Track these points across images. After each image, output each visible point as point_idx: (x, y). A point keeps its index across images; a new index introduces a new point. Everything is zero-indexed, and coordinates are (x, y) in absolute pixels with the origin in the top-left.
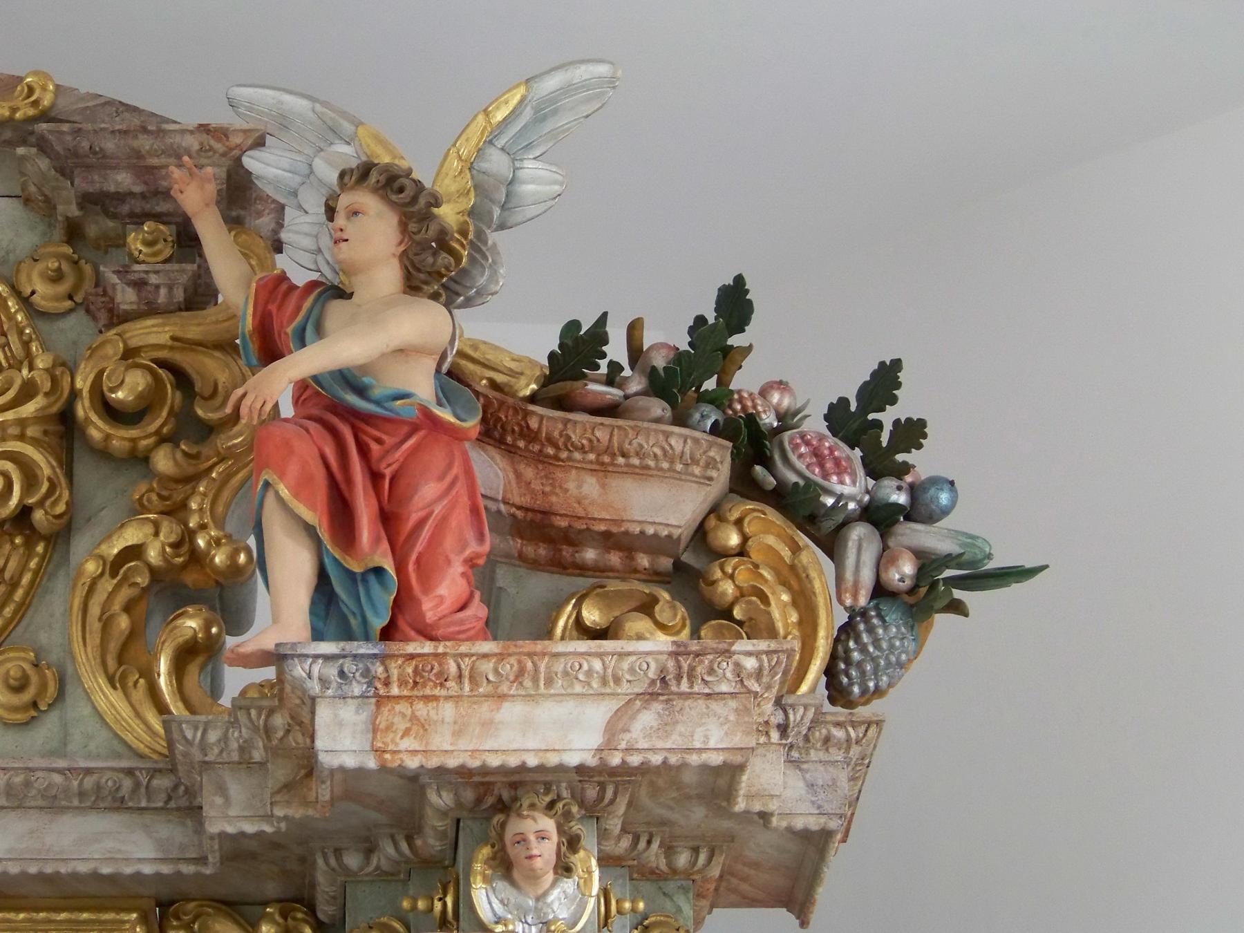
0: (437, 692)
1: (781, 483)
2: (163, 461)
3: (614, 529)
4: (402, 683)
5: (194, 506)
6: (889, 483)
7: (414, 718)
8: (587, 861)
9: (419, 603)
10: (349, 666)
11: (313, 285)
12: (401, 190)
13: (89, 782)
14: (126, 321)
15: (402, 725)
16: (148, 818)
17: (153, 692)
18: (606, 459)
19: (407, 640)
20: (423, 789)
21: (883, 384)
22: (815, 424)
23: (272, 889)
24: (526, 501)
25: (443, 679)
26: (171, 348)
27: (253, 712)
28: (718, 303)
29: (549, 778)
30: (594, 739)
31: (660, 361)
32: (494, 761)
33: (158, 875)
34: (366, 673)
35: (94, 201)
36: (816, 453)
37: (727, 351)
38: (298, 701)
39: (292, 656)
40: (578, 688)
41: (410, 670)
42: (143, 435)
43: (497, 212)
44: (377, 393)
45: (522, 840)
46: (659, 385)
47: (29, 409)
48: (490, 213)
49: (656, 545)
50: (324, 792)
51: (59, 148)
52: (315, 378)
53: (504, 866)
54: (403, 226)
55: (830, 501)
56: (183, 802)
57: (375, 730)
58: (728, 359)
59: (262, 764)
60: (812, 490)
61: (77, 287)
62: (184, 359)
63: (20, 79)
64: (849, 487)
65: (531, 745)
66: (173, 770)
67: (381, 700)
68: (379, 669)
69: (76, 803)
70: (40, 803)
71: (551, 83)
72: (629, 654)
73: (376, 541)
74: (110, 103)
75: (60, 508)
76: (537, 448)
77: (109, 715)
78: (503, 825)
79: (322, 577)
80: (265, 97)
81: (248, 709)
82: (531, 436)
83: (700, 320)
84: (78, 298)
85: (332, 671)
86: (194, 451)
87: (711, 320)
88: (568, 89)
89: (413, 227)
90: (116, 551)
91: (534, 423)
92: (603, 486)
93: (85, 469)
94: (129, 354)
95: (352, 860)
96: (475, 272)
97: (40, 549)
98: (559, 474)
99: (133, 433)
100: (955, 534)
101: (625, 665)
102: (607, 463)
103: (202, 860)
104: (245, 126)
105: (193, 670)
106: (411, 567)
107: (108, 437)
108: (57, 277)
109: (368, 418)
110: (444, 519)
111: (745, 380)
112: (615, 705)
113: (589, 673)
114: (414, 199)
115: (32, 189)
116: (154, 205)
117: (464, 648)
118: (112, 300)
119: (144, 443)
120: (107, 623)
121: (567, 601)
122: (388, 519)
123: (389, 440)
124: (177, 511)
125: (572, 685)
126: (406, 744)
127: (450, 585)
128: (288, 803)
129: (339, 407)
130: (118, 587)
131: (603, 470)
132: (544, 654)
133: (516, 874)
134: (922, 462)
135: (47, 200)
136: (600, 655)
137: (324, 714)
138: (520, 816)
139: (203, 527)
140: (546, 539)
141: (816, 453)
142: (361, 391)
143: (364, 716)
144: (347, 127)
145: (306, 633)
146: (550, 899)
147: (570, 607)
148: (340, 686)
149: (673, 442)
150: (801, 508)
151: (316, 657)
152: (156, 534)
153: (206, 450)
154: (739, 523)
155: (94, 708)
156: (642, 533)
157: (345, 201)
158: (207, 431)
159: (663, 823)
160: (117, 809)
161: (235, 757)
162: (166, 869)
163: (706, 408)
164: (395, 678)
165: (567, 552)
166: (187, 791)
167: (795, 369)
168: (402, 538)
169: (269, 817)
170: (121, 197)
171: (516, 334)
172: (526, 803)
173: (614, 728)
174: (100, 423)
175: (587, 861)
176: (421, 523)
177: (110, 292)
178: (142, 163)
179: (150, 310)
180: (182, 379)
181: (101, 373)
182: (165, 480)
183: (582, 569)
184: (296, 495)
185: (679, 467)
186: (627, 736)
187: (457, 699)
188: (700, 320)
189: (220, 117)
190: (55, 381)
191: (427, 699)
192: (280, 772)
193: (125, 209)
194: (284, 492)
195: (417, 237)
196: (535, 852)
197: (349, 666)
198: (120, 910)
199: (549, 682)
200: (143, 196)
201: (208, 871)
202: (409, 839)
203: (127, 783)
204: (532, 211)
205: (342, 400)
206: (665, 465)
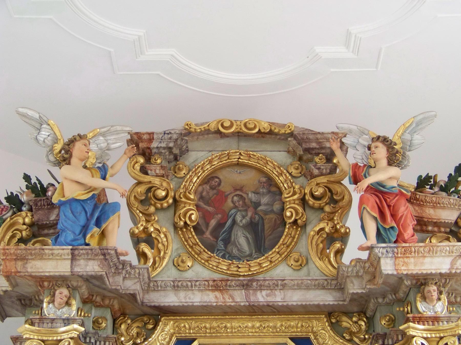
0: (409, 255)
2: (327, 209)
3: (438, 221)
4: (401, 254)
5: (335, 218)
7: (404, 262)
8: (444, 297)
9: (404, 234)
10: (389, 250)
12: (387, 141)
13: (317, 282)
14: (315, 177)
15: (401, 264)
16: (331, 291)
17: (330, 261)
18: (435, 205)
19: (400, 243)
20: (403, 280)
23: (355, 309)
25: (411, 252)
26: (327, 183)
27: (361, 263)
28: (455, 170)
29: (433, 277)
30: (448, 266)
32: (425, 272)
33: (333, 304)
34: (393, 251)
35: (307, 150)
37: (458, 181)
38: (374, 259)
39: (375, 247)
40: (443, 254)
41: (403, 250)
42: (321, 203)
43: (408, 147)
45: (429, 292)
47: (296, 197)
48: (406, 148)
49: (445, 225)
50: (381, 281)
51: (299, 138)
52: (371, 184)
53: (424, 298)
54: (388, 150)
56: (339, 287)
57: (395, 265)
59: (361, 276)
60: (171, 334)
62: (331, 186)
65: (433, 268)
66: (337, 279)
67: (396, 258)
68: (396, 250)
69: (313, 287)
70: (305, 288)
72: (455, 246)
73: (391, 221)
74: (307, 129)
75: (304, 220)
76: (419, 202)
77: (319, 267)
78: (424, 288)
79: (378, 230)
81: (360, 262)
82: (417, 200)
83: (450, 175)
84: (302, 173)
85: (384, 251)
86: (334, 206)
87: (453, 175)
89: (390, 150)
90: (318, 229)
91: (418, 197)
92: (435, 211)
93: (307, 209)
95: (380, 300)
96: (404, 161)
97: (299, 229)
98: (424, 209)
99: (320, 202)
101: (455, 248)
102: (435, 206)
103: (344, 301)
104: (342, 132)
105: (338, 256)
106: (400, 226)
107: (314, 203)
108: (297, 169)
109: (386, 193)
110: (406, 216)
112: (452, 258)
113: (446, 251)
115: (291, 149)
117: (416, 245)
118: (312, 173)
119: (322, 205)
120: (317, 245)
121: (427, 238)
122: (393, 216)
123: (391, 198)
124: (332, 220)
125: (441, 254)
126: (403, 268)
127: (410, 231)
128: (370, 285)
129: (377, 190)
130: (319, 237)
131: (434, 207)
132: (435, 246)
133: (427, 300)
135: (294, 151)
136: (449, 246)
137: (382, 261)
138: (428, 286)
139: (338, 223)
140: (422, 225)
142: (384, 187)
143: (392, 261)
144: (366, 132)
145: (376, 243)
146: (436, 306)
147: (428, 240)
148: (386, 254)
149: (451, 200)
151: (381, 247)
152: (328, 225)
153: (337, 206)
155: (316, 265)
156: (445, 222)
157: (373, 145)
158: (336, 202)
159: (456, 290)
160: (323, 289)
161: (355, 274)
162: (336, 303)
164: (399, 252)
165: (424, 228)
166: (340, 284)
168: (397, 220)
169: (364, 289)
170: (313, 149)
172: (430, 283)
173: (453, 263)
174: (312, 200)
175: (444, 297)
176: (402, 216)
177: (311, 171)
178: (318, 141)
179: (322, 174)
180: (330, 191)
181: (312, 189)
182: (329, 213)
183: (428, 232)
184: (371, 210)
185: (452, 206)
186: (456, 266)
187: (414, 257)
188: (450, 175)
189: (336, 130)
190: (301, 191)
191: (407, 257)
192: (367, 278)
193: (314, 152)
195: (391, 153)
196: (433, 294)
197: (389, 250)
198: (320, 315)
199: (436, 253)
200: (318, 149)
201: (345, 303)
202: (395, 294)
203: (326, 283)
205: (378, 188)
206: (449, 206)
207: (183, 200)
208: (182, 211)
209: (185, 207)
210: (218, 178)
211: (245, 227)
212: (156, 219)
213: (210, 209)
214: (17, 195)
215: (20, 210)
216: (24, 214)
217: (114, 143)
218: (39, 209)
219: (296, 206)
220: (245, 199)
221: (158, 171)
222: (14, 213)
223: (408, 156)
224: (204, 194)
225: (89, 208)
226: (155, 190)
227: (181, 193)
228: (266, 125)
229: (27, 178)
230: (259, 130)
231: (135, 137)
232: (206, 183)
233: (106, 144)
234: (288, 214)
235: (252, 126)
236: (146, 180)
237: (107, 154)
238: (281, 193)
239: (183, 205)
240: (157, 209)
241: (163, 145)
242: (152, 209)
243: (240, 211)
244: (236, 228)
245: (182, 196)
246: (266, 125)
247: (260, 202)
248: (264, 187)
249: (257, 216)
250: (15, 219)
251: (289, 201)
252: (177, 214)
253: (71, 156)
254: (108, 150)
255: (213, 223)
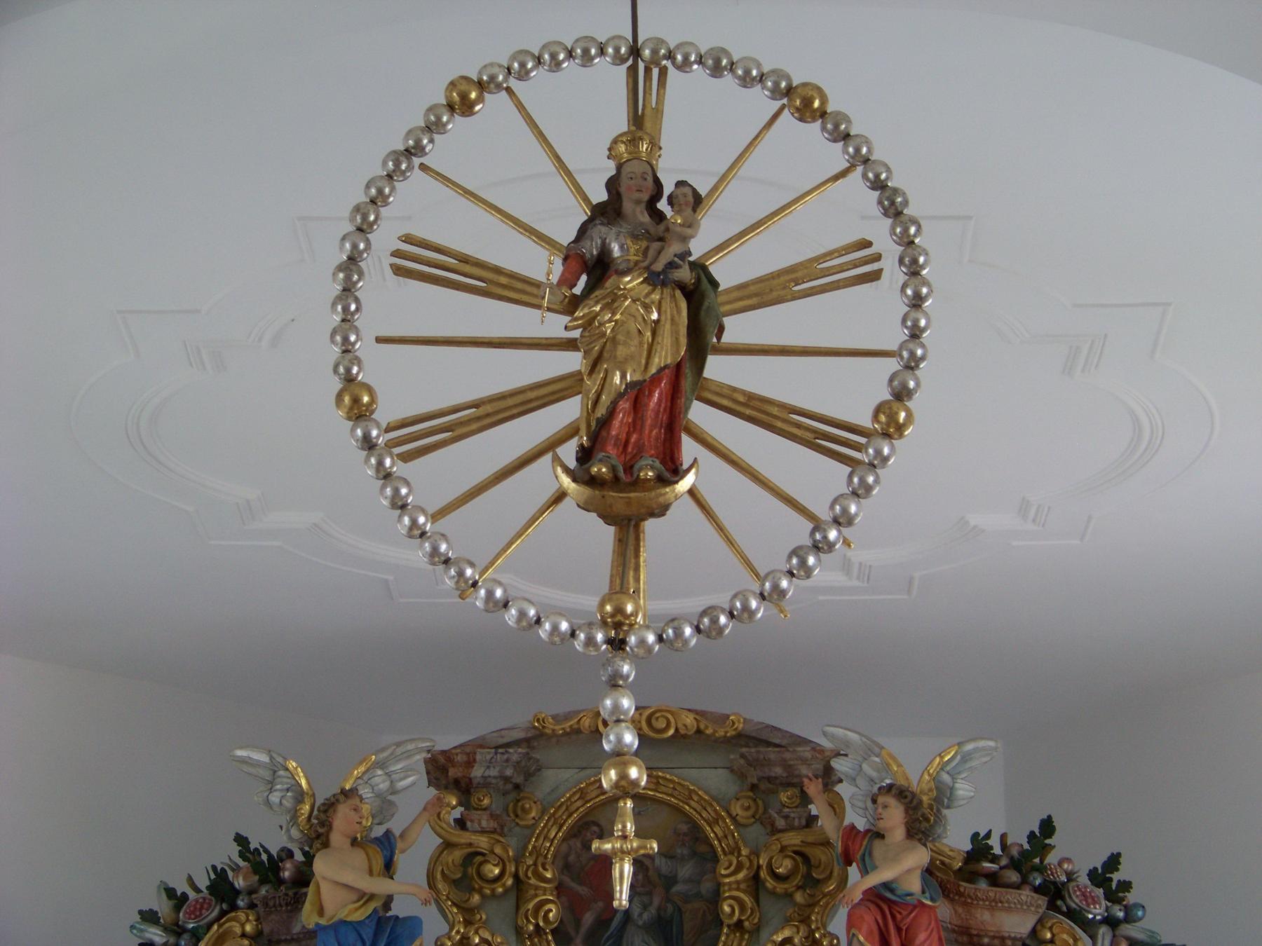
1: (1068, 907)
2: (799, 897)
6: (1117, 907)
11: (867, 831)
21: (1113, 862)
22: (1083, 880)
24: (959, 923)
31: (1015, 852)
35: (769, 779)
36: (1084, 895)
44: (899, 892)
46: (1015, 864)
47: (741, 876)
54: (906, 811)
55: (1090, 916)
58: (1047, 849)
61: (756, 812)
62: (807, 850)
63: (728, 716)
64: (1096, 912)
71: (969, 747)
74: (768, 726)
80: (839, 732)
82: (961, 894)
83: (1032, 833)
88: (976, 750)
90: (573, 485)
93: (763, 898)
94: (783, 849)
100: (1144, 930)
102: (994, 905)
109: (894, 902)
111: (1052, 859)
114: (911, 802)
116: (793, 782)
123: (905, 913)
124: (805, 920)
129: (881, 898)
131: (992, 909)
134: (1131, 897)
139: (818, 928)
141: (1084, 895)
142: (892, 891)
144: (877, 750)
150: (1075, 915)
154: (1051, 929)
157: (881, 800)
163: (1036, 874)
167: (1075, 853)
171: (956, 839)
181: (771, 858)
184: (866, 939)
188: (1032, 833)
190: (751, 861)
194: (861, 938)
204: (962, 802)
207: (533, 881)
208: (531, 906)
209: (536, 895)
210: (598, 825)
211: (647, 928)
212: (484, 917)
213: (583, 890)
214: (223, 869)
215: (234, 907)
216: (242, 916)
217: (401, 779)
218: (271, 912)
219: (742, 895)
220: (647, 869)
221: (484, 823)
222: (223, 913)
223: (945, 817)
224: (572, 858)
225: (368, 934)
226: (481, 864)
227: (529, 867)
228: (689, 720)
229: (241, 840)
230: (677, 730)
231: (442, 760)
232: (575, 836)
233: (387, 784)
234: (727, 909)
235: (661, 724)
236: (463, 841)
237: (391, 803)
238: (716, 860)
239: (532, 892)
240: (483, 896)
241: (493, 772)
242: (476, 898)
243: (640, 894)
244: (631, 928)
245: (530, 874)
246: (689, 720)
247: (676, 876)
248: (684, 845)
249: (669, 905)
250: (227, 925)
251: (729, 883)
252: (522, 911)
253: (330, 827)
254: (394, 793)
255: (588, 919)
